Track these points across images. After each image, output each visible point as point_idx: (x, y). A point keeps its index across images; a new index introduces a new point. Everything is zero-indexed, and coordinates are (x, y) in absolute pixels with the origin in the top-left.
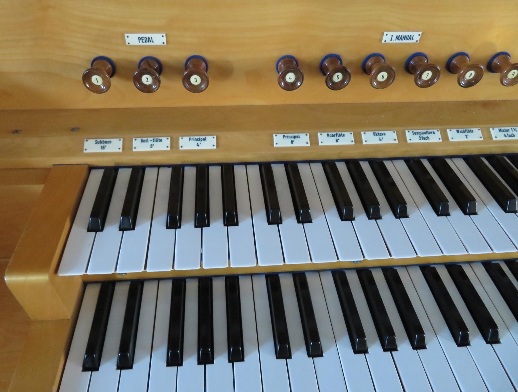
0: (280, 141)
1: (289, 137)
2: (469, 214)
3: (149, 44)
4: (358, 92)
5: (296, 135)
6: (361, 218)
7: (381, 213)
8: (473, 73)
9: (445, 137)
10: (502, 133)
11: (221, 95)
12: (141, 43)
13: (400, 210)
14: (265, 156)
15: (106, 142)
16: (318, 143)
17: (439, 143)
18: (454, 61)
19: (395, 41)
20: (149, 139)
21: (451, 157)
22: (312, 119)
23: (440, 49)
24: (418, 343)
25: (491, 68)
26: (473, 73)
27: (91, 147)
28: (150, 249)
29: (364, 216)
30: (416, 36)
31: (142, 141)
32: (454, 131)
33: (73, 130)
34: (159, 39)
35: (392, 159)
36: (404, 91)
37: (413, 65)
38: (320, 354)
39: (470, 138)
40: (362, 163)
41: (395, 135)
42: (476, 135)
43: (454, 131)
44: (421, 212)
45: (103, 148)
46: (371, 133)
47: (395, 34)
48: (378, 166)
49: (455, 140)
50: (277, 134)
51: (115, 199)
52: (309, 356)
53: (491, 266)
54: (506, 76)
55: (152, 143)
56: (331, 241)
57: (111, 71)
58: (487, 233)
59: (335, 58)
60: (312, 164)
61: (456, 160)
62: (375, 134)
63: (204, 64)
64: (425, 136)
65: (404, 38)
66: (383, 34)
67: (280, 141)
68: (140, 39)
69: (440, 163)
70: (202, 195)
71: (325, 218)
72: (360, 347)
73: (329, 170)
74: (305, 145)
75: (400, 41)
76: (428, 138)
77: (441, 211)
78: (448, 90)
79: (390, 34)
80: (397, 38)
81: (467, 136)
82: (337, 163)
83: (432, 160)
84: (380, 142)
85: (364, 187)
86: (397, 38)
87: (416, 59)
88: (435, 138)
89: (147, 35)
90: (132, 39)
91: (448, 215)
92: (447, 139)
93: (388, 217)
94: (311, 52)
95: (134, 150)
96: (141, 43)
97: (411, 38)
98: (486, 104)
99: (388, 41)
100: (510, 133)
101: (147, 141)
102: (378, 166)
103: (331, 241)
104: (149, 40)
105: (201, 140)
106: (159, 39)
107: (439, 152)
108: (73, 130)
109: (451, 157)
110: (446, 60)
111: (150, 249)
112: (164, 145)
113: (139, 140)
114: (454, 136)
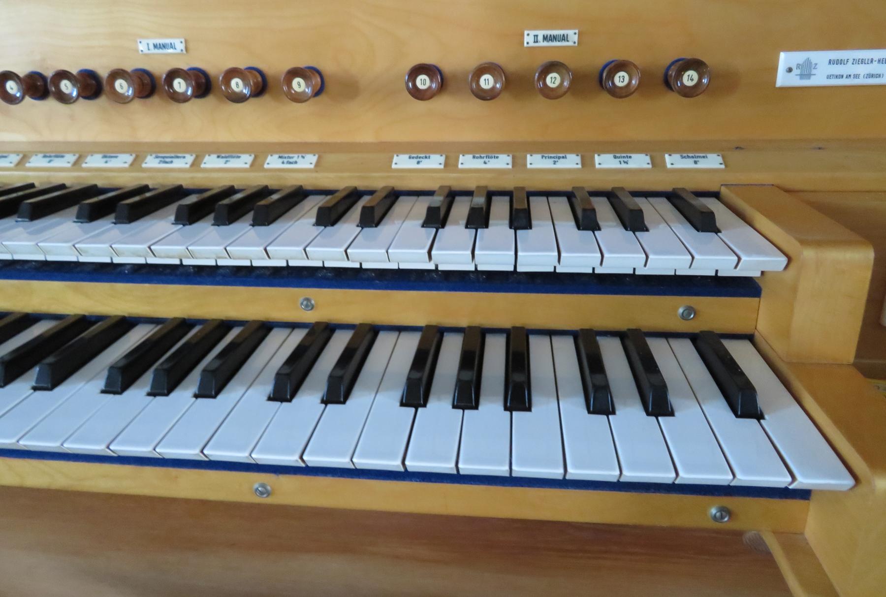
1: (551, 157)
5: (561, 155)
16: (525, 165)
17: (578, 169)
19: (542, 44)
30: (573, 36)
33: (737, 148)
41: (578, 159)
45: (555, 163)
47: (541, 33)
57: (318, 87)
58: (18, 241)
63: (319, 79)
66: (523, 35)
74: (505, 166)
75: (161, 51)
76: (172, 162)
79: (145, 42)
81: (555, 163)
86: (545, 38)
97: (564, 38)
108: (737, 148)
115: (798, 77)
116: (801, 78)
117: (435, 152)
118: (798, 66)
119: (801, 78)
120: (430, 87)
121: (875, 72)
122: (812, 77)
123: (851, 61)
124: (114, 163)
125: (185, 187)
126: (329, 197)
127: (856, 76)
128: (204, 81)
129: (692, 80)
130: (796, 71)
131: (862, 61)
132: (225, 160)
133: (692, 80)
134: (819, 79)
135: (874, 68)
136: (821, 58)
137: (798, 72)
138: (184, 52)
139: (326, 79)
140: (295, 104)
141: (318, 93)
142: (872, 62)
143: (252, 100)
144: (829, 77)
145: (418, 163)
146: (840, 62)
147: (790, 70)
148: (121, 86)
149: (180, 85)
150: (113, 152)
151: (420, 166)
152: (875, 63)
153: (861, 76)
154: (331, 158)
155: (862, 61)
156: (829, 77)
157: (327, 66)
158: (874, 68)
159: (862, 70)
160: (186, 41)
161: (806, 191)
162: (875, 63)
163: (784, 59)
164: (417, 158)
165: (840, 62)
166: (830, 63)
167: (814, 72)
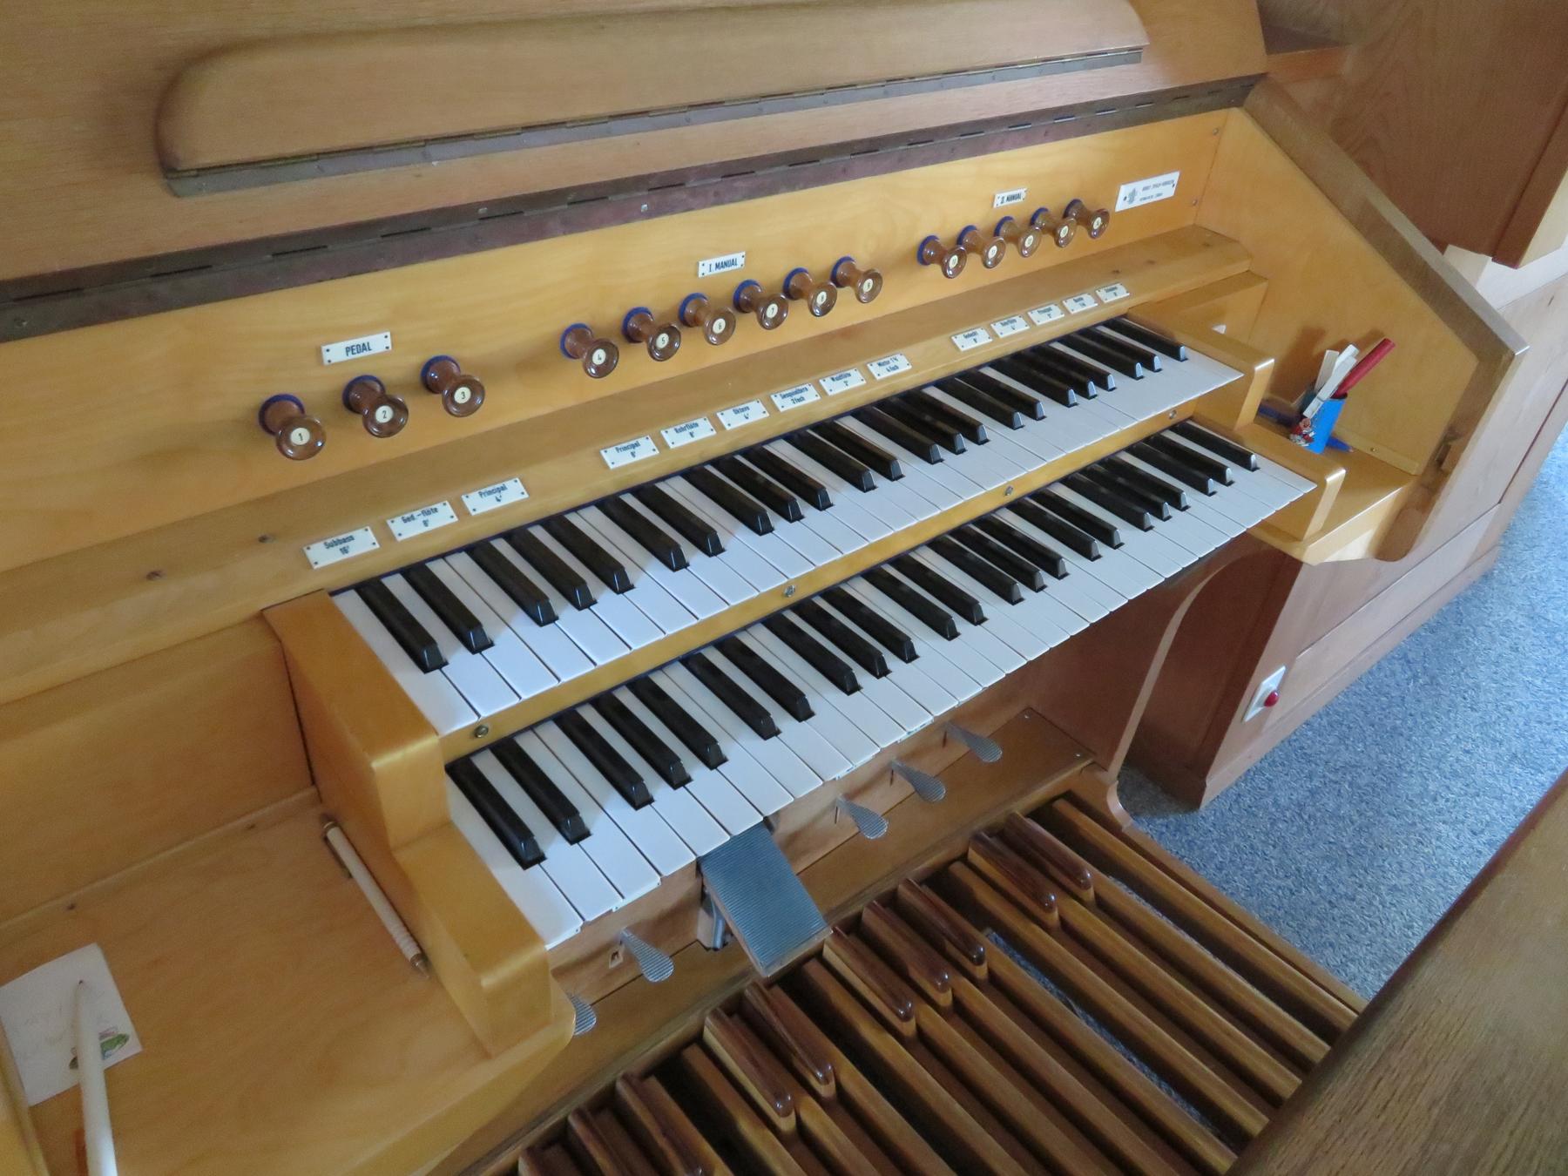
0: (616, 458)
1: (490, 493)
2: (621, 592)
3: (366, 353)
4: (695, 355)
6: (567, 614)
7: (594, 595)
8: (823, 294)
9: (718, 426)
10: (884, 368)
11: (511, 406)
12: (351, 356)
13: (618, 581)
14: (606, 487)
15: (344, 541)
18: (792, 283)
19: (715, 271)
20: (415, 514)
21: (663, 479)
22: (629, 416)
23: (771, 272)
24: (576, 833)
25: (631, 336)
26: (823, 294)
27: (322, 555)
28: (520, 669)
29: (463, 652)
30: (740, 258)
31: (406, 520)
32: (828, 380)
33: (263, 539)
34: (379, 342)
35: (575, 509)
36: (750, 339)
37: (745, 301)
38: (586, 834)
39: (695, 438)
40: (387, 582)
42: (855, 380)
43: (828, 380)
44: (648, 573)
46: (730, 412)
48: (418, 575)
49: (678, 445)
50: (467, 493)
51: (421, 613)
52: (572, 843)
53: (936, 545)
54: (1024, 247)
55: (423, 518)
56: (753, 570)
59: (639, 313)
60: (449, 558)
61: (671, 481)
62: (737, 412)
64: (797, 396)
65: (726, 264)
67: (616, 458)
68: (348, 349)
69: (648, 493)
70: (549, 566)
71: (513, 633)
72: (638, 798)
73: (613, 511)
77: (675, 562)
78: (800, 324)
79: (707, 262)
80: (717, 266)
82: (430, 565)
83: (637, 491)
84: (499, 505)
85: (757, 486)
86: (717, 266)
87: (747, 290)
88: (704, 430)
89: (360, 341)
90: (336, 353)
91: (686, 565)
92: (723, 428)
93: (606, 599)
94: (609, 314)
95: (400, 539)
96: (351, 356)
97: (733, 262)
98: (847, 333)
99: (707, 273)
100: (892, 364)
101: (412, 518)
102: (418, 575)
103: (753, 570)
104: (365, 347)
105: (499, 490)
106: (379, 342)
107: (822, 414)
109: (663, 479)
110: (620, 324)
111: (520, 669)
112: (444, 515)
113: (398, 520)
114: (833, 387)
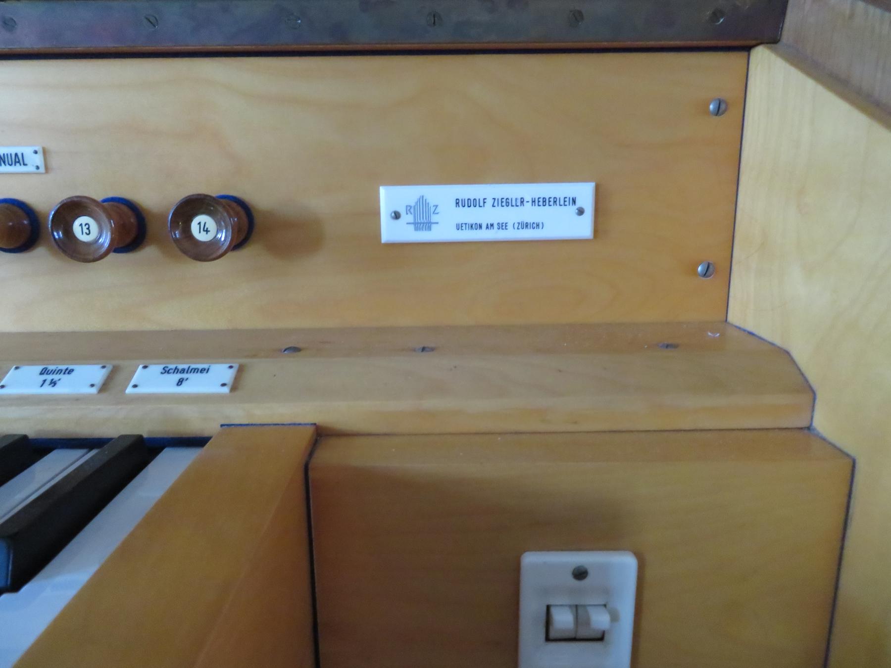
5: (200, 366)
115: (412, 227)
116: (416, 229)
117: (86, 359)
118: (409, 209)
119: (416, 229)
120: (96, 241)
121: (530, 220)
122: (434, 226)
123: (489, 202)
124: (66, 387)
125: (145, 436)
126: (93, 452)
127: (502, 226)
128: (133, 220)
129: (207, 231)
130: (406, 218)
131: (506, 202)
132: (178, 376)
133: (207, 231)
134: (444, 230)
135: (529, 213)
136: (443, 195)
137: (410, 218)
138: (42, 170)
139: (258, 220)
140: (199, 264)
141: (240, 241)
142: (522, 202)
143: (112, 256)
144: (459, 227)
145: (180, 382)
146: (472, 203)
147: (397, 216)
148: (85, 229)
149: (204, 228)
150: (64, 360)
151: (184, 389)
152: (528, 205)
153: (510, 226)
154: (262, 370)
155: (506, 202)
156: (459, 227)
157: (261, 197)
158: (529, 213)
159: (511, 215)
160: (45, 152)
161: (369, 435)
162: (528, 205)
163: (389, 198)
164: (176, 370)
165: (472, 203)
166: (457, 203)
167: (434, 218)
